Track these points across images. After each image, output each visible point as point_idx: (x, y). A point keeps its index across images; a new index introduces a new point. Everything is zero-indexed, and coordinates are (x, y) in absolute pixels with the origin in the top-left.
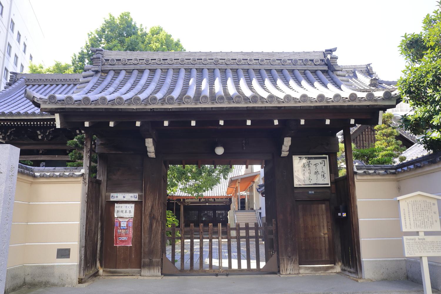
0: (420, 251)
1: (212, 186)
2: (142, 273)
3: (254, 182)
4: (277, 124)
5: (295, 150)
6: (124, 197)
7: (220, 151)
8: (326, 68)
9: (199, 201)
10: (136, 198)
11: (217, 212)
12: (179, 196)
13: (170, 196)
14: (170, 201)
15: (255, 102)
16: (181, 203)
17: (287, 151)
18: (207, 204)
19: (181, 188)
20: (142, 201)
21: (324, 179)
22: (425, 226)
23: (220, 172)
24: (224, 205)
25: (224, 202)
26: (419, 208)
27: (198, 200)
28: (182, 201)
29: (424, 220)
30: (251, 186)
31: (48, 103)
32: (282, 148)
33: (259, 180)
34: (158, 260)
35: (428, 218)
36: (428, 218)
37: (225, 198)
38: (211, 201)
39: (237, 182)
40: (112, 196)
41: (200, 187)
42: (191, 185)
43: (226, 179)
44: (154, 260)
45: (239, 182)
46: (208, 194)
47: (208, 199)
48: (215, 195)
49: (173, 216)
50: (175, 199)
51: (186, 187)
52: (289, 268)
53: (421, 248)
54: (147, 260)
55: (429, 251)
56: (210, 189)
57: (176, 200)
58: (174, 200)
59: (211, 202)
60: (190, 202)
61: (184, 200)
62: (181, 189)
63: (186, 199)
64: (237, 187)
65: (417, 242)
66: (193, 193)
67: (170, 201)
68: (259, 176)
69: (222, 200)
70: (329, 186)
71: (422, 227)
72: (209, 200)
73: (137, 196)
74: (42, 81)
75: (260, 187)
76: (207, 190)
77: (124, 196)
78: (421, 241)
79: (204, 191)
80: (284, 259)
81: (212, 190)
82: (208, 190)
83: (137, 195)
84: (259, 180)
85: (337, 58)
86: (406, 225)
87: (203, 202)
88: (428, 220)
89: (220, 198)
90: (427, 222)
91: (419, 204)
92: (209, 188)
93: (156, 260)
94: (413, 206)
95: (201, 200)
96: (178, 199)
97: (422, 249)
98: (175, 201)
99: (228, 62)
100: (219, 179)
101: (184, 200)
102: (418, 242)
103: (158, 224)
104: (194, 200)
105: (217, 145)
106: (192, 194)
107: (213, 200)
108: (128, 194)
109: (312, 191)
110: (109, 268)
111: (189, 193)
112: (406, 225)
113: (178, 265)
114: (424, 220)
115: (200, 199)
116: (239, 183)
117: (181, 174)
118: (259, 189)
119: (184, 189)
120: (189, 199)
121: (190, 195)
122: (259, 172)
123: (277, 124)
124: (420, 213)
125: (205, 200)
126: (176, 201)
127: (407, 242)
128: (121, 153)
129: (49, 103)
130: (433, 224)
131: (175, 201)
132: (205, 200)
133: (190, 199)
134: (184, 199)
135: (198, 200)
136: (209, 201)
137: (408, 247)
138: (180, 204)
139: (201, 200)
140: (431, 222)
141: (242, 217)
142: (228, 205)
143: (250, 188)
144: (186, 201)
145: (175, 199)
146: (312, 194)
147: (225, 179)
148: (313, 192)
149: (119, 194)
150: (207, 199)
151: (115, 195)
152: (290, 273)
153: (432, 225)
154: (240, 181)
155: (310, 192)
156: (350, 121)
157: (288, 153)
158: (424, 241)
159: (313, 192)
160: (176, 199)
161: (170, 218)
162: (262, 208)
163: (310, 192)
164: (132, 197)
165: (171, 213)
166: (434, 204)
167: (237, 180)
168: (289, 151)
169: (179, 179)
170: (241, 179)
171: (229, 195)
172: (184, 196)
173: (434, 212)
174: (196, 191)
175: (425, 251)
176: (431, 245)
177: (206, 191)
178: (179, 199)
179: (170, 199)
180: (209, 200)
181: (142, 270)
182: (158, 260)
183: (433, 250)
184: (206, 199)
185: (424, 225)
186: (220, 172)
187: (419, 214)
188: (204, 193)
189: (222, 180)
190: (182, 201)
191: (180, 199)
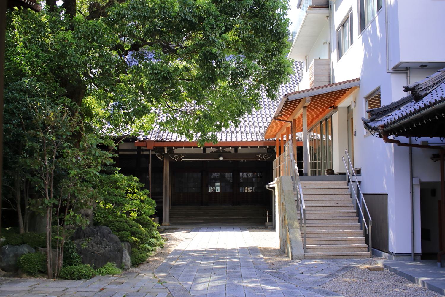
1: (239, 116)
3: (335, 108)
9: (202, 152)
11: (241, 174)
12: (160, 141)
13: (139, 141)
14: (142, 153)
16: (165, 155)
18: (221, 159)
19: (160, 120)
23: (259, 82)
24: (260, 162)
25: (258, 154)
27: (201, 151)
28: (166, 152)
30: (326, 119)
33: (355, 102)
37: (260, 147)
38: (230, 152)
39: (300, 105)
41: (210, 119)
42: (185, 112)
43: (273, 98)
45: (304, 107)
46: (227, 135)
47: (224, 147)
48: (240, 140)
49: (142, 189)
50: (150, 147)
51: (175, 119)
56: (233, 125)
57: (152, 151)
58: (149, 150)
59: (229, 155)
60: (183, 154)
61: (170, 149)
62: (161, 124)
63: (176, 148)
64: (294, 120)
66: (191, 132)
67: (142, 153)
68: (355, 91)
69: (254, 151)
72: (226, 149)
75: (374, 117)
76: (225, 126)
79: (219, 128)
81: (236, 126)
82: (226, 127)
84: (355, 102)
87: (211, 155)
89: (251, 147)
92: (230, 122)
95: (208, 151)
96: (157, 148)
98: (151, 153)
100: (257, 97)
101: (170, 149)
104: (192, 151)
106: (188, 135)
107: (233, 151)
110: (163, 185)
111: (181, 134)
115: (205, 150)
116: (306, 109)
117: (159, 80)
118: (372, 120)
119: (167, 122)
120: (182, 147)
121: (184, 138)
122: (357, 82)
125: (215, 149)
126: (154, 153)
131: (151, 153)
132: (215, 149)
133: (185, 147)
134: (171, 147)
135: (201, 151)
136: (226, 152)
138: (162, 159)
139: (208, 151)
141: (314, 192)
142: (267, 161)
143: (321, 122)
144: (176, 151)
145: (150, 147)
147: (273, 99)
150: (221, 149)
154: (307, 104)
156: (362, 71)
160: (152, 148)
161: (135, 195)
162: (362, 171)
165: (135, 181)
167: (300, 100)
169: (154, 95)
170: (313, 98)
171: (270, 140)
172: (170, 141)
174: (199, 128)
177: (224, 129)
178: (159, 148)
179: (142, 148)
180: (226, 149)
184: (218, 147)
186: (259, 82)
188: (219, 134)
189: (265, 100)
190: (166, 152)
191: (162, 149)
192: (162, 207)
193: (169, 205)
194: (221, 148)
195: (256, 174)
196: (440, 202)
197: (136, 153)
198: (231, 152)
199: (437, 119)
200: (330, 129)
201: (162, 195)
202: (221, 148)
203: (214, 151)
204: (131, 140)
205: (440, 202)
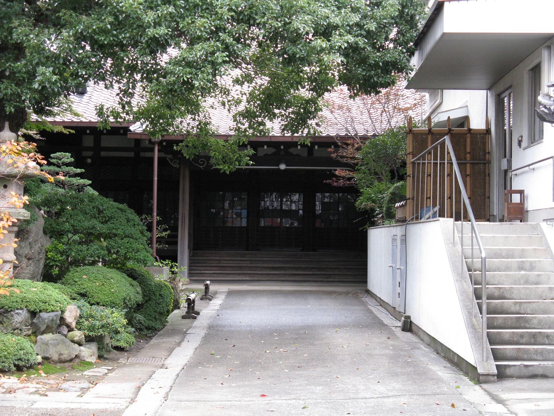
18: (283, 167)
72: (292, 150)
125: (272, 150)
132: (272, 150)
136: (292, 154)
180: (292, 150)
192: (177, 251)
193: (189, 247)
194: (282, 147)
195: (337, 195)
196: (505, 157)
197: (132, 154)
198: (300, 156)
199: (83, 170)
200: (290, 279)
201: (177, 231)
202: (282, 147)
203: (270, 153)
204: (88, 132)
205: (505, 157)
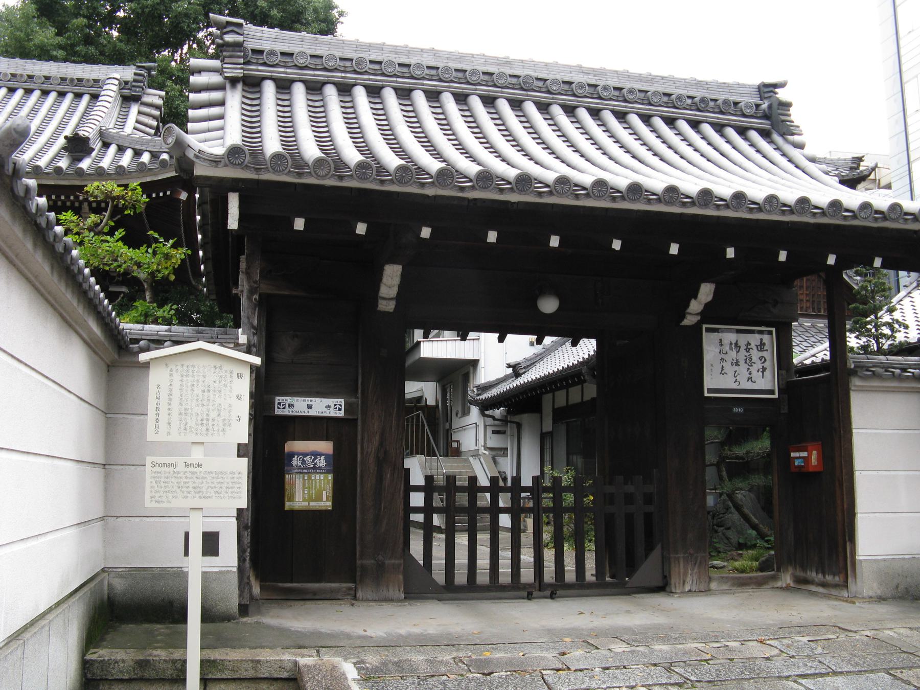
0: (186, 494)
2: (360, 594)
4: (733, 256)
5: (715, 315)
6: (309, 407)
7: (549, 305)
8: (764, 124)
10: (340, 410)
15: (706, 206)
17: (697, 314)
20: (356, 420)
21: (763, 380)
22: (207, 430)
26: (201, 384)
29: (208, 415)
31: (222, 164)
32: (688, 306)
34: (397, 562)
35: (219, 411)
36: (219, 411)
40: (279, 404)
44: (387, 562)
52: (689, 579)
53: (187, 487)
54: (369, 562)
55: (209, 494)
65: (178, 473)
70: (776, 396)
71: (199, 432)
73: (343, 404)
74: (18, 78)
77: (310, 403)
78: (192, 469)
80: (678, 559)
83: (341, 401)
85: (787, 105)
86: (157, 427)
88: (219, 415)
90: (213, 420)
91: (201, 374)
93: (393, 561)
94: (185, 379)
97: (191, 489)
99: (580, 91)
102: (184, 473)
103: (396, 476)
105: (543, 292)
108: (319, 399)
109: (739, 406)
112: (157, 427)
113: (439, 575)
114: (208, 415)
123: (733, 256)
124: (200, 398)
127: (153, 472)
128: (286, 293)
129: (226, 165)
130: (230, 425)
137: (154, 484)
140: (224, 420)
146: (738, 414)
148: (741, 410)
149: (296, 398)
151: (288, 400)
152: (690, 591)
153: (227, 428)
155: (735, 410)
157: (699, 318)
158: (198, 469)
159: (741, 410)
163: (735, 410)
164: (328, 407)
166: (240, 376)
168: (702, 313)
173: (237, 396)
175: (197, 495)
176: (215, 481)
181: (359, 587)
182: (397, 562)
183: (217, 492)
185: (204, 428)
187: (197, 400)
